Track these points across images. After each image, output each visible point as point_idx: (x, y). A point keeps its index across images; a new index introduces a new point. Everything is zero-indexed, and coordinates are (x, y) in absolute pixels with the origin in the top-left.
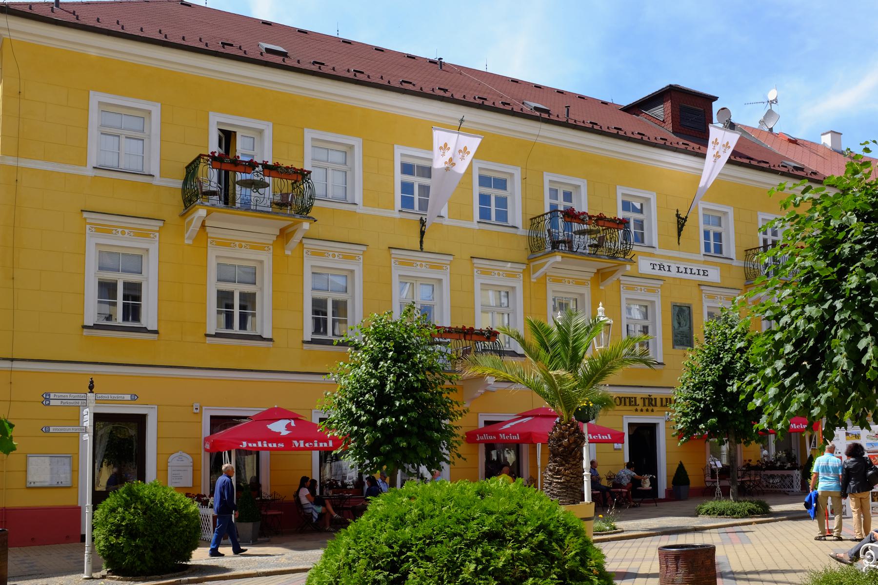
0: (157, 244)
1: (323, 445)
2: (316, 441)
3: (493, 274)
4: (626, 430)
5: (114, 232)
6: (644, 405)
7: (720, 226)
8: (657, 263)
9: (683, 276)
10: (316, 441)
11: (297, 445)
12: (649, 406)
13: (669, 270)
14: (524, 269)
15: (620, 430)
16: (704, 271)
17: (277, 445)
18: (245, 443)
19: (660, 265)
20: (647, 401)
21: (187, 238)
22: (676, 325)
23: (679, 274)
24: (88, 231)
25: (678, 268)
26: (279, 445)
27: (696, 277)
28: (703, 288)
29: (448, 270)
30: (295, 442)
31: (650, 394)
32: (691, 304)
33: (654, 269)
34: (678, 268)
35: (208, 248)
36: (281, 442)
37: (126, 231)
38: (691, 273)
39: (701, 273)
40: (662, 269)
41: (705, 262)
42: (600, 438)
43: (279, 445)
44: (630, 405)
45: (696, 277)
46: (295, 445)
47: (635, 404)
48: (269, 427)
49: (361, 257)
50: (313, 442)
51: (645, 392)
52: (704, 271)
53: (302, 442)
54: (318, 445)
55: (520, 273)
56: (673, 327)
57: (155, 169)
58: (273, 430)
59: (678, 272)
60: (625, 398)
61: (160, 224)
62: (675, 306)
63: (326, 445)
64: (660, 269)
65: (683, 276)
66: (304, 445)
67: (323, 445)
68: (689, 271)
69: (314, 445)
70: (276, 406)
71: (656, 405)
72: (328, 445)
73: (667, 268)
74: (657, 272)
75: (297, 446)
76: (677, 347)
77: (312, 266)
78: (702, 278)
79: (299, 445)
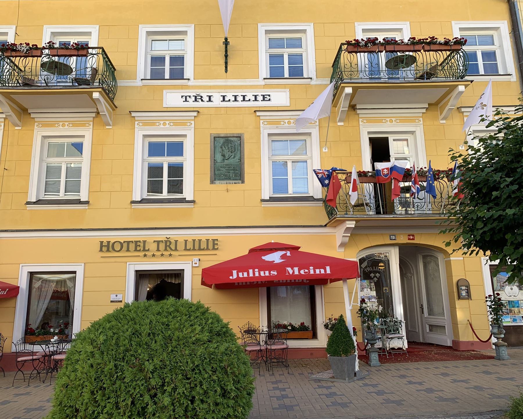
0: (91, 130)
1: (243, 275)
2: (311, 268)
3: (157, 124)
4: (23, 283)
5: (282, 123)
6: (158, 250)
7: (493, 44)
8: (192, 95)
9: (232, 104)
10: (311, 268)
11: (291, 272)
12: (166, 250)
13: (210, 100)
14: (94, 118)
15: (13, 283)
16: (263, 96)
17: (270, 273)
18: (235, 272)
19: (196, 97)
20: (162, 246)
21: (339, 121)
22: (219, 158)
23: (224, 103)
24: (261, 125)
25: (224, 97)
26: (272, 272)
27: (252, 104)
28: (258, 114)
29: (193, 125)
30: (289, 270)
31: (168, 237)
32: (241, 134)
33: (186, 101)
34: (224, 97)
35: (360, 126)
36: (273, 270)
37: (393, 119)
38: (244, 100)
39: (260, 98)
40: (200, 100)
41: (266, 86)
42: (312, 272)
43: (272, 272)
44: (136, 250)
45: (252, 104)
46: (288, 272)
47: (144, 250)
48: (263, 258)
49: (193, 122)
50: (309, 269)
51: (162, 235)
52: (263, 96)
53: (296, 269)
54: (315, 271)
55: (420, 117)
56: (214, 161)
57: (314, 76)
58: (266, 260)
59: (224, 100)
60: (128, 242)
61: (195, 114)
62: (215, 138)
63: (323, 271)
64: (196, 100)
65: (232, 104)
66: (299, 272)
67: (243, 275)
68: (240, 98)
69: (309, 272)
70: (273, 242)
71: (176, 249)
72: (325, 271)
73: (206, 99)
74: (191, 103)
75: (291, 273)
76: (217, 182)
77: (369, 133)
78: (260, 103)
79: (294, 272)
